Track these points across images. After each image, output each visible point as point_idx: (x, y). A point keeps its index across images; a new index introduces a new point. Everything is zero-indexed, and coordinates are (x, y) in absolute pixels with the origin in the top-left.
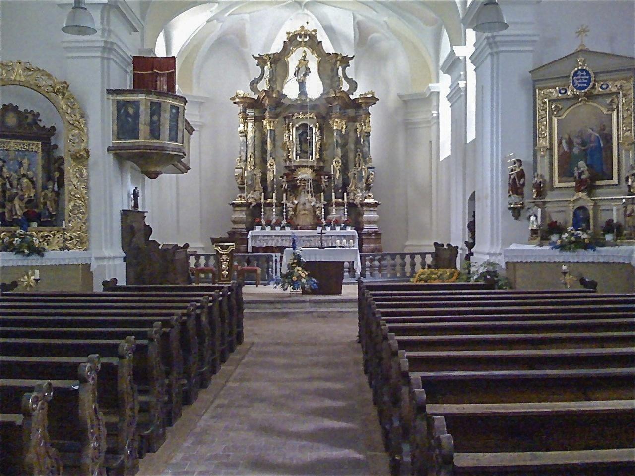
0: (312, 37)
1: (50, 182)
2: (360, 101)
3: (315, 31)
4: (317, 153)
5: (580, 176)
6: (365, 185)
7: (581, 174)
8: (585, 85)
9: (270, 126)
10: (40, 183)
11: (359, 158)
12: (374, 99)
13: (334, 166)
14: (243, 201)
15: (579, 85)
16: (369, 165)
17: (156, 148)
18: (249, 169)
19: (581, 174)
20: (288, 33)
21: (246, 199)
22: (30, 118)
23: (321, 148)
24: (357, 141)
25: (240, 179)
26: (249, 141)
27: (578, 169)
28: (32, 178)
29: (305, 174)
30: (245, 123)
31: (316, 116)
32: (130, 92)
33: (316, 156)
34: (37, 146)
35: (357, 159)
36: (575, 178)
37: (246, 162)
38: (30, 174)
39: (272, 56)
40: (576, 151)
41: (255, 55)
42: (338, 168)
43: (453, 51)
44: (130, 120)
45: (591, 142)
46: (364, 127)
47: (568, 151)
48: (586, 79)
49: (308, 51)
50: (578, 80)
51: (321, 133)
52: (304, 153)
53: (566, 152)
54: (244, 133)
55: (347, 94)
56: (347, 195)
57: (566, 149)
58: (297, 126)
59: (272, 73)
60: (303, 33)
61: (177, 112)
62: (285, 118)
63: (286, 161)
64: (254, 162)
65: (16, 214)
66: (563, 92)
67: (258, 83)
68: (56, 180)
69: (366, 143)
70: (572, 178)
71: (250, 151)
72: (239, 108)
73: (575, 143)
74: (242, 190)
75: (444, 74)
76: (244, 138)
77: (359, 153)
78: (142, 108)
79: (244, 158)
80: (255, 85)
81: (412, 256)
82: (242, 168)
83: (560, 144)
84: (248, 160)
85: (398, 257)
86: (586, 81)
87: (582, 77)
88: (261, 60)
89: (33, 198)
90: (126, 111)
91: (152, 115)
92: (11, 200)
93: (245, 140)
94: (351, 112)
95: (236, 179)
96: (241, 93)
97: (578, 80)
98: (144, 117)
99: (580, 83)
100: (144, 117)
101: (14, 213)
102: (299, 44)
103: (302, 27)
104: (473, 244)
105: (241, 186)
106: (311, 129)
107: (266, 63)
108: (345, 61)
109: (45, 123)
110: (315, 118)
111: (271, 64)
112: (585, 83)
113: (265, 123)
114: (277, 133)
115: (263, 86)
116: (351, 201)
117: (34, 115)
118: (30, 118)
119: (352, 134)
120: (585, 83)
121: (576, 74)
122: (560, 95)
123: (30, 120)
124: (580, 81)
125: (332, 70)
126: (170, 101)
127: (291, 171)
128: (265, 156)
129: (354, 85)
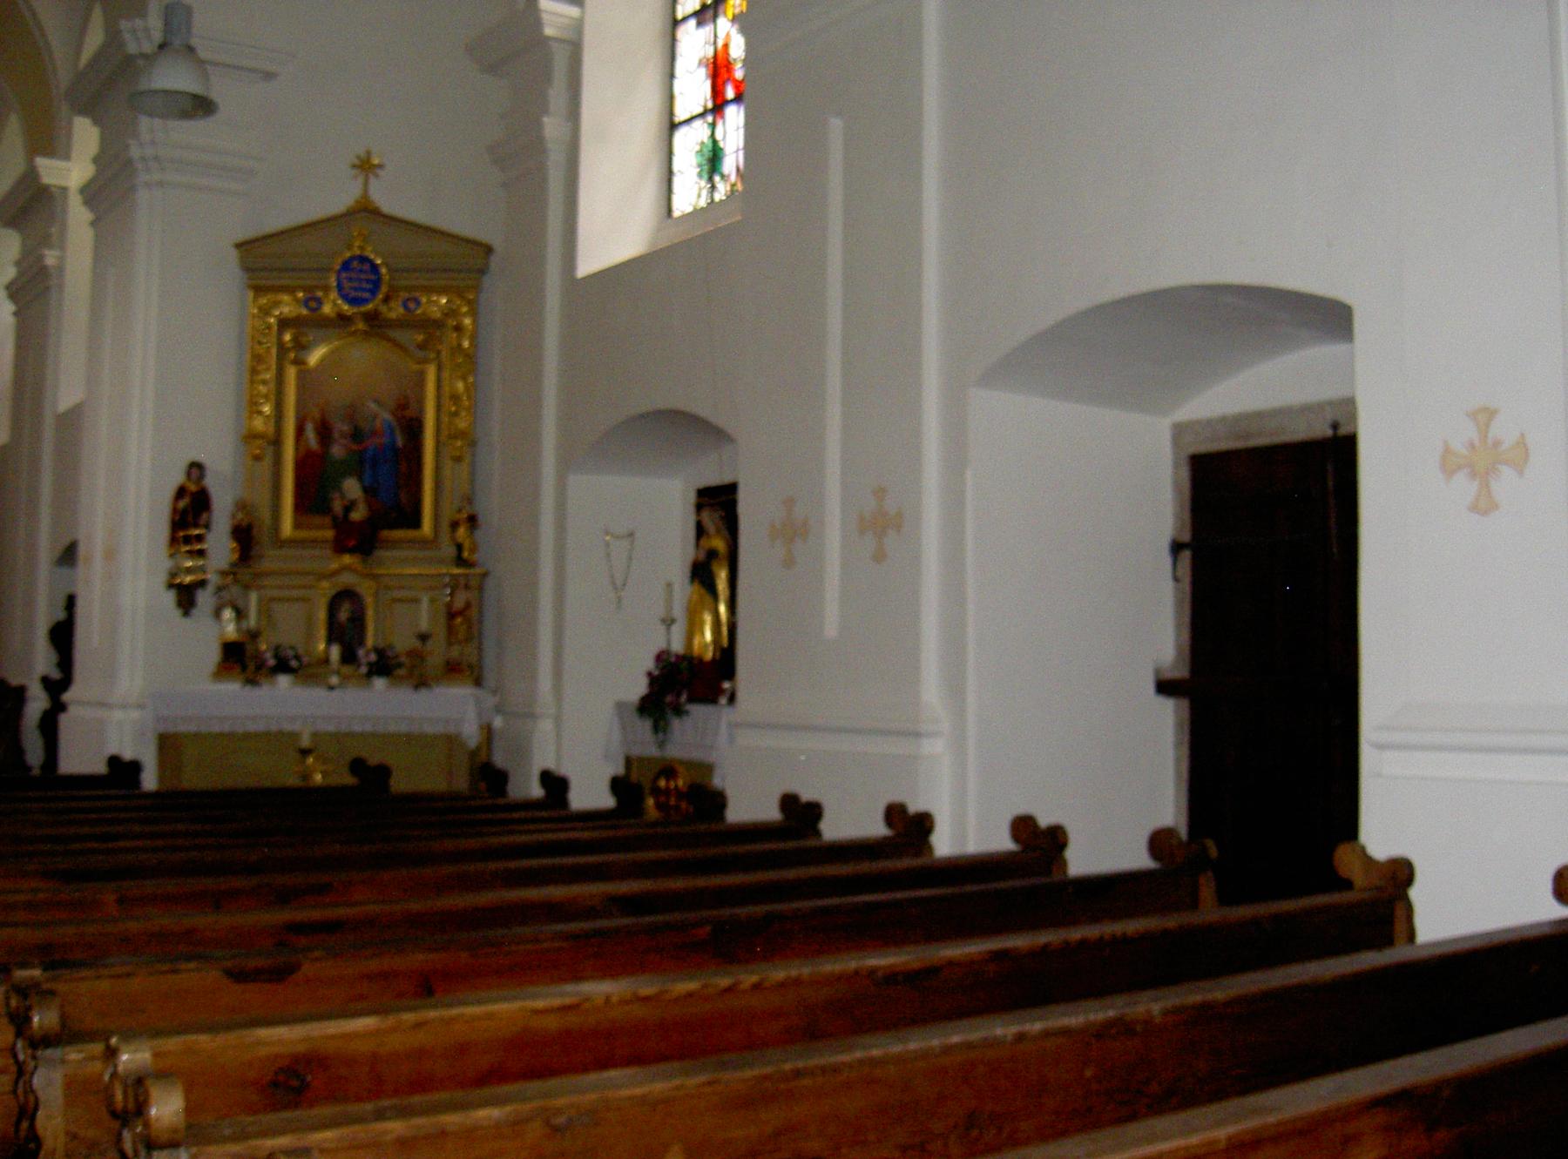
8: (367, 295)
15: (353, 294)
27: (343, 497)
40: (337, 451)
43: (31, 175)
48: (368, 281)
50: (350, 279)
66: (313, 304)
70: (327, 520)
73: (336, 435)
83: (300, 431)
87: (363, 276)
99: (356, 289)
120: (364, 290)
121: (346, 266)
124: (355, 284)
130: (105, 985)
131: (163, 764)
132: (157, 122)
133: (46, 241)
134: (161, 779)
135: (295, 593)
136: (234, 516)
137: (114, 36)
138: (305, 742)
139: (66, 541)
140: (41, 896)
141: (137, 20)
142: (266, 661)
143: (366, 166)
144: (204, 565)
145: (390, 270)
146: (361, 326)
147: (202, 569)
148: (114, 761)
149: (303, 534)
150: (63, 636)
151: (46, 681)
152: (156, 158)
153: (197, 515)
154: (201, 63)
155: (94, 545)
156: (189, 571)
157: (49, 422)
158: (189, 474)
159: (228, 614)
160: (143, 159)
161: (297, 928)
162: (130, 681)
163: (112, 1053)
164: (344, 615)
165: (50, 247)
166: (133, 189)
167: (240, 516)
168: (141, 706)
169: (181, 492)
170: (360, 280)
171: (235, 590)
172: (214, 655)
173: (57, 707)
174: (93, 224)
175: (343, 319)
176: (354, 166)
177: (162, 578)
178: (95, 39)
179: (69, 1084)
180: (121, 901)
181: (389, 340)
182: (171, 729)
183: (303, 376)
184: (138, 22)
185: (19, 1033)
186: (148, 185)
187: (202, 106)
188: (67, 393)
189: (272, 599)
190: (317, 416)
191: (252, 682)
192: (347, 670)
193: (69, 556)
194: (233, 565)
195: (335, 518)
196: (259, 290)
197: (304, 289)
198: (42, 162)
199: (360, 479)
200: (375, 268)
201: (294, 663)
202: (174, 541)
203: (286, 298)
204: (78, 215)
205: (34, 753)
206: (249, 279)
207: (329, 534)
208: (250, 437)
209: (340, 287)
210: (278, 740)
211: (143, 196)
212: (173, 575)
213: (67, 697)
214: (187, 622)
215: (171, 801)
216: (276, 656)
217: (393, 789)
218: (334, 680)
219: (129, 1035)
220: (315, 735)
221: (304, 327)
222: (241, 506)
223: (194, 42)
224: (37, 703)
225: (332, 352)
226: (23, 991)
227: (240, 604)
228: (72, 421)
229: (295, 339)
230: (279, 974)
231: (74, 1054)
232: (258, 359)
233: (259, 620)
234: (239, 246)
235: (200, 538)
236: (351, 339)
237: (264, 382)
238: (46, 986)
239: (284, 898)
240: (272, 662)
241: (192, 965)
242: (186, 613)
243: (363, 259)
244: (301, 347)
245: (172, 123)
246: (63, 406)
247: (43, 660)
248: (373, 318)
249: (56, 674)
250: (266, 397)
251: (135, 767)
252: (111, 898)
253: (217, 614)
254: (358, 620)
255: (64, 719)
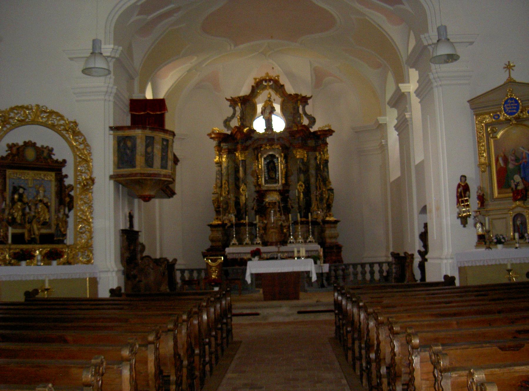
0: (276, 82)
1: (62, 206)
2: (319, 133)
3: (278, 76)
4: (284, 179)
5: (516, 188)
6: (325, 205)
7: (516, 186)
8: (515, 111)
9: (241, 157)
10: (53, 209)
11: (320, 182)
12: (330, 132)
13: (298, 190)
14: (220, 222)
15: (510, 111)
16: (328, 188)
17: (150, 175)
18: (224, 194)
19: (516, 186)
20: (255, 79)
21: (222, 220)
22: (46, 152)
23: (286, 173)
24: (318, 168)
25: (216, 203)
26: (224, 171)
27: (514, 181)
28: (47, 203)
29: (273, 198)
30: (220, 156)
31: (281, 147)
32: (129, 128)
33: (282, 181)
34: (51, 177)
35: (317, 183)
36: (512, 189)
37: (222, 189)
38: (45, 200)
39: (242, 99)
40: (511, 166)
41: (227, 98)
42: (301, 191)
43: (398, 89)
44: (128, 152)
45: (523, 158)
46: (323, 156)
47: (504, 167)
48: (514, 106)
49: (273, 93)
50: (508, 106)
51: (286, 162)
52: (272, 178)
53: (503, 167)
54: (219, 164)
55: (307, 128)
56: (311, 215)
57: (502, 165)
58: (265, 156)
59: (242, 113)
60: (267, 78)
61: (166, 146)
62: (254, 149)
63: (255, 186)
64: (228, 188)
65: (34, 234)
66: (496, 117)
67: (230, 121)
68: (67, 205)
69: (326, 170)
70: (509, 190)
71: (224, 178)
72: (214, 143)
73: (509, 160)
74: (218, 212)
75: (391, 108)
76: (220, 168)
77: (319, 177)
78: (138, 141)
79: (219, 185)
80: (227, 123)
81: (372, 265)
82: (218, 193)
83: (497, 160)
84: (224, 186)
85: (351, 267)
86: (515, 108)
87: (512, 105)
88: (233, 102)
89: (47, 220)
90: (125, 143)
91: (147, 146)
92: (30, 222)
93: (220, 170)
94: (311, 143)
95: (213, 203)
96: (217, 129)
97: (508, 106)
98: (140, 148)
99: (510, 110)
100: (140, 148)
101: (32, 233)
102: (265, 88)
103: (267, 74)
104: (426, 252)
105: (218, 210)
106: (278, 158)
107: (237, 104)
108: (305, 100)
109: (58, 156)
110: (280, 148)
111: (241, 105)
112: (514, 109)
113: (237, 154)
114: (247, 162)
115: (235, 123)
116: (314, 220)
117: (49, 150)
118: (46, 152)
119: (312, 162)
120: (514, 109)
121: (506, 102)
122: (494, 120)
123: (45, 154)
124: (510, 108)
125: (294, 108)
126: (162, 135)
127: (261, 194)
128: (237, 183)
129: (313, 121)
130: (459, 351)
131: (460, 278)
132: (437, 66)
133: (405, 110)
134: (460, 283)
135: (500, 216)
136: (477, 192)
137: (419, 41)
138: (509, 267)
139: (423, 205)
140: (432, 322)
141: (425, 34)
142: (493, 240)
143: (509, 67)
144: (469, 210)
145: (521, 102)
146: (514, 122)
147: (469, 211)
148: (446, 277)
149: (502, 196)
150: (424, 236)
151: (419, 252)
152: (438, 77)
153: (465, 193)
154: (452, 43)
155: (432, 207)
156: (464, 212)
157: (413, 168)
158: (461, 179)
159: (478, 225)
160: (434, 78)
161: (519, 332)
162: (448, 250)
163: (471, 375)
164: (518, 223)
165: (407, 112)
166: (432, 88)
167: (479, 192)
168: (452, 258)
169: (459, 186)
170: (512, 106)
171: (480, 217)
172: (476, 239)
173: (424, 260)
174: (420, 102)
175: (508, 121)
176: (504, 68)
177: (456, 215)
178: (412, 43)
179: (452, 385)
180: (457, 323)
181: (525, 125)
182: (462, 265)
183: (496, 141)
184: (426, 35)
185: (435, 367)
186: (437, 86)
187: (452, 58)
188: (418, 157)
189: (492, 219)
190: (503, 155)
191: (489, 248)
192: (522, 241)
193: (424, 210)
194: (479, 208)
195: (512, 189)
196: (477, 115)
197: (493, 113)
198: (400, 85)
199: (520, 175)
200: (517, 102)
201: (503, 240)
202: (458, 202)
203: (487, 116)
204: (415, 101)
205: (418, 276)
206: (474, 112)
207: (511, 195)
208: (480, 165)
209: (505, 110)
210: (499, 267)
211: (435, 90)
212: (459, 214)
213: (427, 257)
214: (465, 229)
215: (465, 290)
216: (496, 238)
217: (300, 293)
218: (517, 245)
219: (479, 368)
220: (512, 264)
221: (496, 124)
222: (480, 188)
223: (449, 37)
224: (417, 259)
225: (506, 132)
226: (437, 354)
227: (483, 222)
228: (421, 167)
229: (491, 130)
230: (518, 347)
231: (454, 375)
232: (480, 138)
233: (489, 227)
234: (468, 101)
235: (467, 201)
236: (511, 127)
237: (483, 146)
238: (443, 352)
239: (513, 322)
240: (495, 240)
241: (488, 345)
242: (464, 226)
243: (512, 99)
244: (494, 132)
245: (442, 65)
246: (417, 162)
247: (418, 245)
248: (518, 119)
249: (423, 249)
250: (484, 151)
251: (453, 279)
252: (455, 322)
253: (475, 226)
254: (524, 224)
255: (426, 264)
